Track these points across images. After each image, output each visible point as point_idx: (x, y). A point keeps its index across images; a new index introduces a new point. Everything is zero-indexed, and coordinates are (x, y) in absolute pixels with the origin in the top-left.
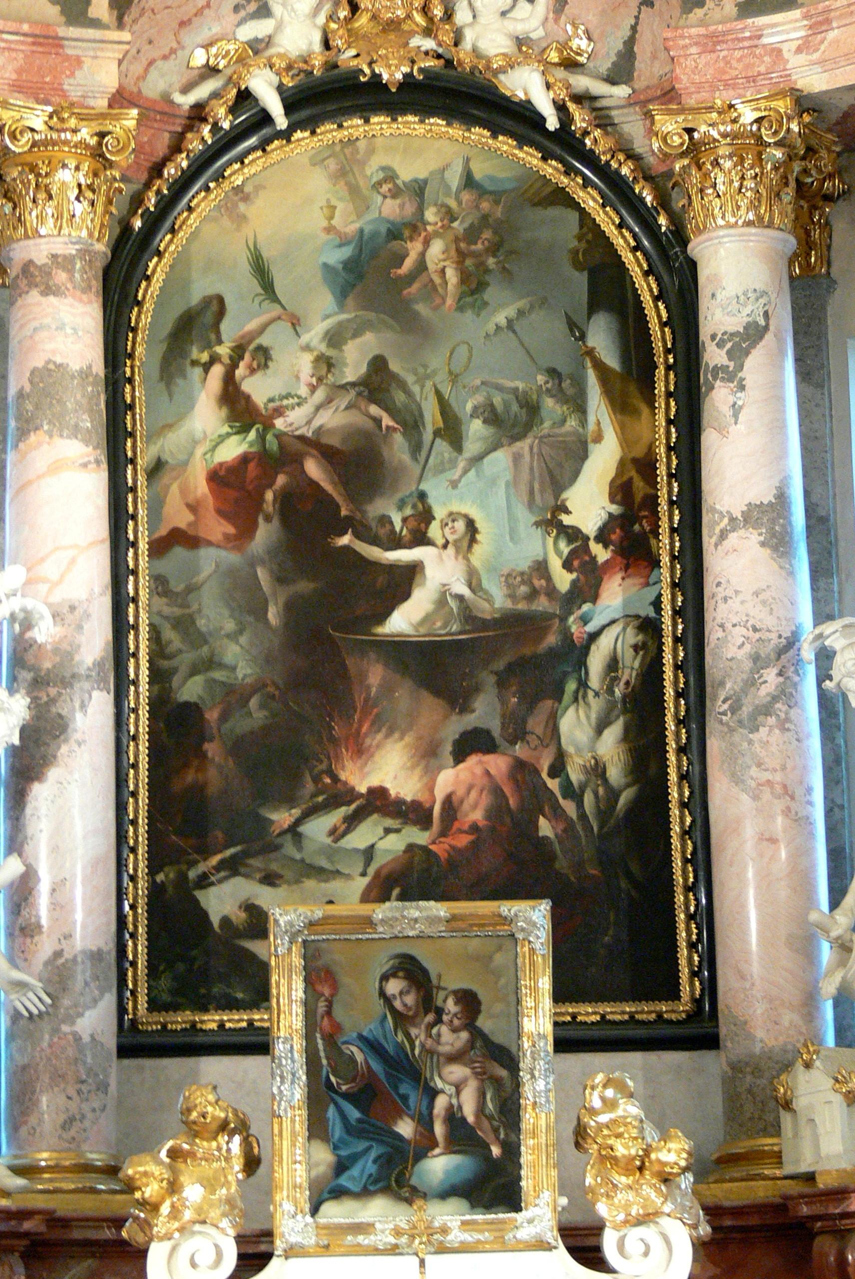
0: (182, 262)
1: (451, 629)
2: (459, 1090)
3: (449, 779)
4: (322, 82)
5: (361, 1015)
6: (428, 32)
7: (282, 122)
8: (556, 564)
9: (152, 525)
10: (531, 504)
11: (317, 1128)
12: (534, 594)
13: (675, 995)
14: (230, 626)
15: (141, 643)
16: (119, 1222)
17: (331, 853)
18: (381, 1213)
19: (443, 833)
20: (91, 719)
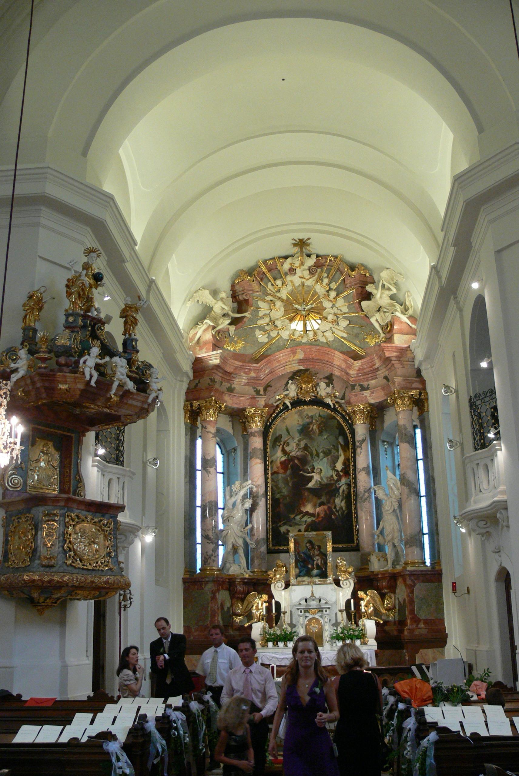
0: (275, 429)
1: (318, 486)
2: (318, 560)
3: (318, 510)
4: (297, 401)
5: (303, 549)
6: (313, 392)
7: (290, 408)
8: (334, 475)
9: (271, 470)
10: (330, 466)
11: (296, 566)
12: (331, 480)
13: (354, 542)
14: (283, 486)
15: (270, 489)
16: (267, 580)
17: (300, 522)
18: (306, 579)
19: (317, 518)
20: (262, 503)
